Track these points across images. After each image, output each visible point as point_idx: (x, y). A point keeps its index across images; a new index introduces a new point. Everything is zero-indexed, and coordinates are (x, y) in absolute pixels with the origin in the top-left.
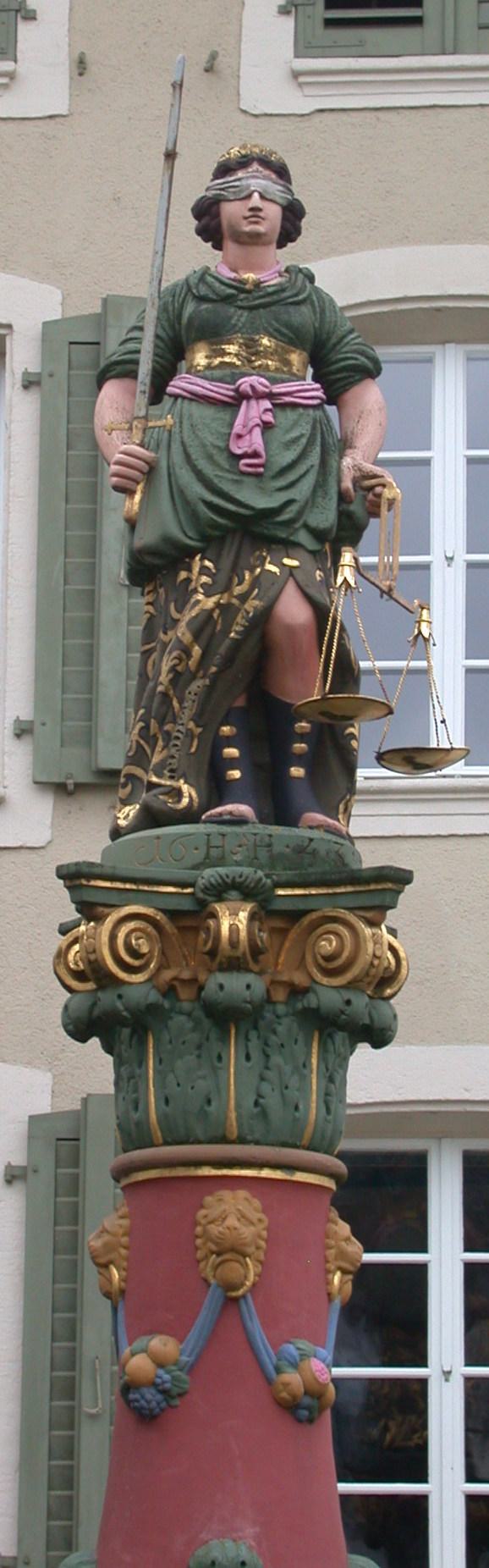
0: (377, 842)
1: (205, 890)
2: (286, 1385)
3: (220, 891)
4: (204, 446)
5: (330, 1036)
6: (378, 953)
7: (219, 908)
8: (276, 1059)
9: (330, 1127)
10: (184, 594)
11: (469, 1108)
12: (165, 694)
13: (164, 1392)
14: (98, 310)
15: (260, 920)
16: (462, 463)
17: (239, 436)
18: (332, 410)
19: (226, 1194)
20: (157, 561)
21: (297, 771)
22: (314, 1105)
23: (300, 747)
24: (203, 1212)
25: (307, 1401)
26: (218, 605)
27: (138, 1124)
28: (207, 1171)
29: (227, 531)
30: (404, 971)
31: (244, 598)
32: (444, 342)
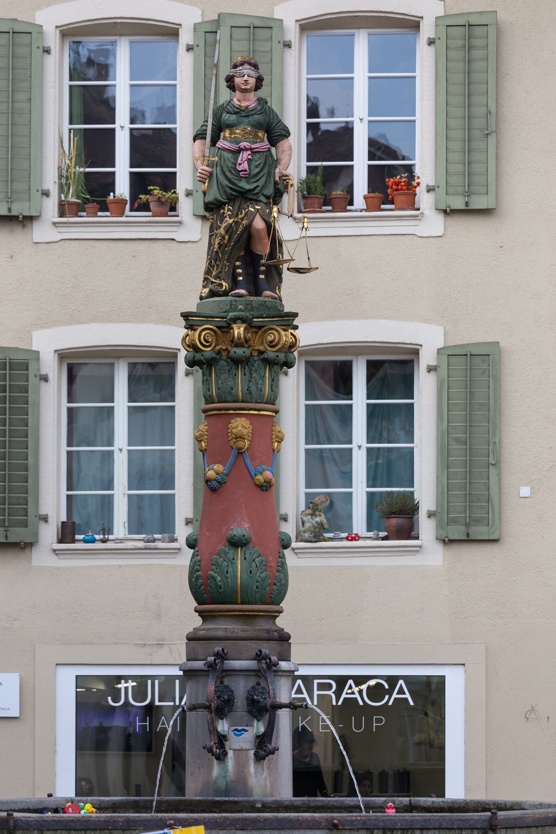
0: (331, 238)
1: (230, 320)
2: (258, 480)
3: (235, 320)
4: (228, 167)
5: (272, 366)
6: (287, 340)
7: (234, 326)
8: (254, 375)
9: (273, 396)
10: (223, 217)
11: (368, 344)
12: (217, 252)
13: (219, 482)
14: (217, 18)
15: (248, 330)
16: (366, 79)
17: (240, 164)
18: (273, 150)
19: (238, 419)
20: (213, 206)
21: (262, 276)
22: (267, 389)
23: (263, 268)
24: (231, 425)
25: (265, 484)
26: (234, 221)
27: (209, 396)
28: (232, 412)
29: (236, 196)
30: (298, 343)
31: (242, 219)
32: (359, 28)
